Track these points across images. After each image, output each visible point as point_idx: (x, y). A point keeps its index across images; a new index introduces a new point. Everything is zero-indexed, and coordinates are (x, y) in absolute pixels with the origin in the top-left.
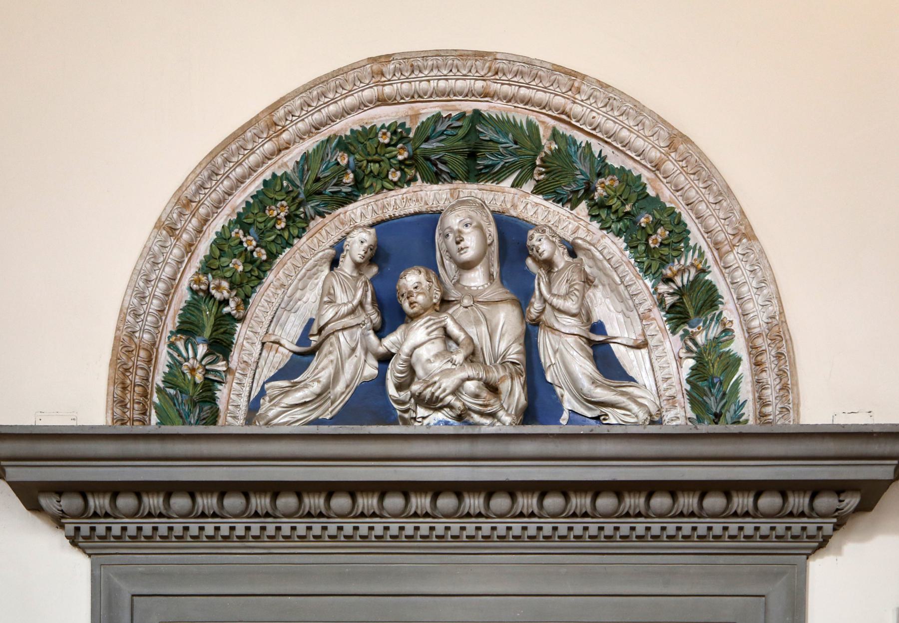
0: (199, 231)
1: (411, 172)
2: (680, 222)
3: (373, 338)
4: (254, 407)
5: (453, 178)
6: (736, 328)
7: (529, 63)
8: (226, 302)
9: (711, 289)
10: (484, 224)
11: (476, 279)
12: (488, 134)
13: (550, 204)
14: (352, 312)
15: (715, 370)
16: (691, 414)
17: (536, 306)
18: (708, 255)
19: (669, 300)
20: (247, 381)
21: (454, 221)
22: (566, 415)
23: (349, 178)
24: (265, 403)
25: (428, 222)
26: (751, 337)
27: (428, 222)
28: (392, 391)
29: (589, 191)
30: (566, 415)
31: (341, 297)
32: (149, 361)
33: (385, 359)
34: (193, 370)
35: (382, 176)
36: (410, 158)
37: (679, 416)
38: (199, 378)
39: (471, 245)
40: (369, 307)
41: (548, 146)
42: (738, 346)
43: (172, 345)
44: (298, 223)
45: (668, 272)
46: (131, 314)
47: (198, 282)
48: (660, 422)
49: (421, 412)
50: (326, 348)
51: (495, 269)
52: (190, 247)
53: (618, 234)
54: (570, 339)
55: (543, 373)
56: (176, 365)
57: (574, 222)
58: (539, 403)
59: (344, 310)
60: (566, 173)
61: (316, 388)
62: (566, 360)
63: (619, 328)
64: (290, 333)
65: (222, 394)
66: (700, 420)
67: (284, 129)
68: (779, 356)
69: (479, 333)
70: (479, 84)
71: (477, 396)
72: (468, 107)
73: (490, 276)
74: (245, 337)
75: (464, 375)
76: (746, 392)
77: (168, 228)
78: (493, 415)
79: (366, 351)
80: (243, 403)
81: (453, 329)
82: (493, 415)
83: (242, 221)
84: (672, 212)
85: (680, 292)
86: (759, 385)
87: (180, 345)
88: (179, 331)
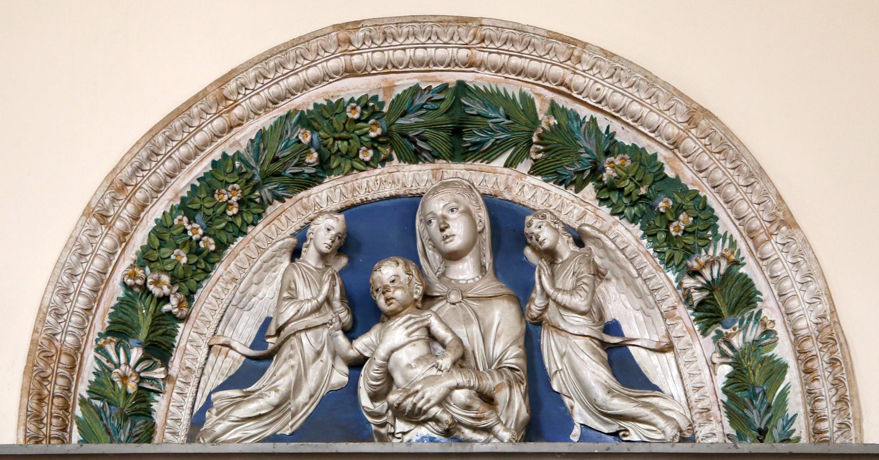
0: (136, 218)
1: (385, 151)
2: (706, 207)
3: (342, 340)
4: (197, 421)
5: (435, 156)
6: (779, 328)
7: (521, 29)
8: (166, 299)
9: (747, 284)
11: (465, 271)
12: (475, 107)
13: (551, 187)
14: (317, 309)
15: (757, 378)
18: (741, 245)
19: (697, 296)
21: (437, 205)
22: (577, 431)
23: (313, 158)
24: (211, 417)
26: (798, 341)
28: (365, 401)
29: (596, 171)
33: (356, 365)
34: (124, 378)
37: (715, 431)
38: (132, 387)
39: (458, 233)
40: (337, 304)
41: (546, 121)
43: (100, 349)
44: (253, 208)
45: (694, 264)
47: (133, 276)
48: (692, 440)
49: (401, 426)
50: (286, 351)
51: (488, 260)
53: (633, 220)
54: (580, 341)
56: (104, 373)
57: (580, 206)
58: (544, 414)
59: (307, 307)
60: (568, 151)
61: (273, 398)
62: (576, 365)
63: (639, 329)
64: (242, 334)
65: (159, 405)
66: (741, 437)
68: (833, 362)
69: (470, 334)
71: (468, 407)
72: (451, 78)
73: (482, 268)
74: (188, 340)
75: (452, 382)
76: (795, 404)
78: (488, 430)
79: (335, 355)
80: (185, 416)
81: (438, 329)
84: (695, 196)
85: (709, 286)
86: (812, 398)
87: (110, 349)
88: (109, 332)
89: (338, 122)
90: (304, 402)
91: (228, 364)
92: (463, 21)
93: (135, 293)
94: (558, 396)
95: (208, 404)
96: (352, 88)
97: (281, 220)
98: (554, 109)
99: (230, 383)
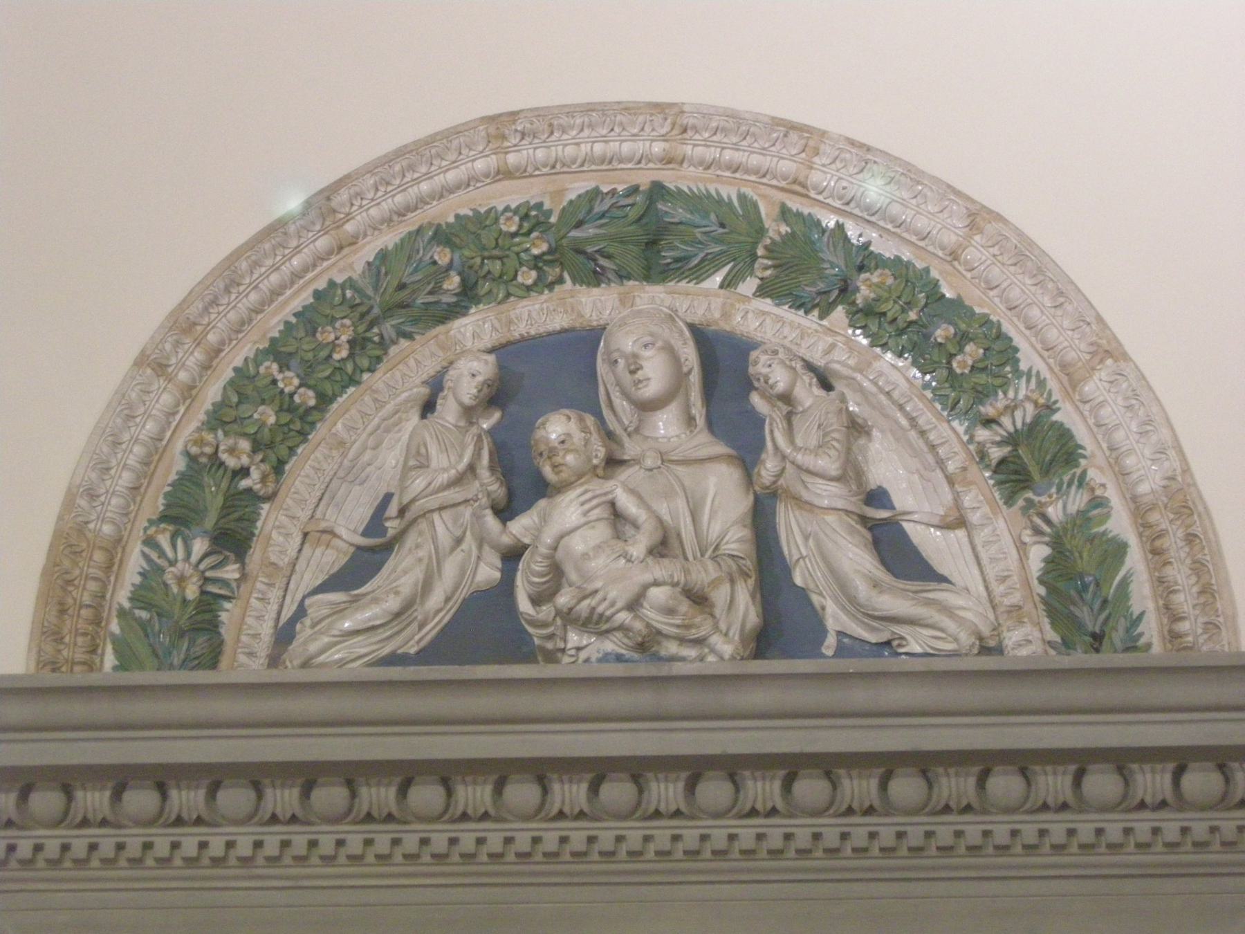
0: (206, 367)
1: (552, 273)
2: (1000, 336)
3: (491, 521)
4: (285, 635)
5: (623, 276)
7: (733, 115)
8: (244, 472)
9: (1064, 435)
10: (677, 344)
11: (665, 425)
13: (785, 312)
14: (458, 481)
15: (1086, 562)
16: (1052, 635)
17: (768, 467)
18: (1052, 384)
19: (996, 453)
20: (274, 595)
22: (831, 640)
24: (304, 630)
25: (582, 345)
26: (1140, 510)
27: (582, 345)
29: (846, 290)
30: (831, 640)
31: (438, 459)
32: (108, 568)
33: (512, 556)
34: (181, 579)
35: (507, 279)
36: (551, 251)
37: (1028, 640)
38: (192, 592)
39: (655, 375)
40: (484, 473)
41: (776, 229)
42: (1120, 524)
43: (150, 542)
44: (369, 349)
45: (988, 410)
46: (83, 494)
47: (200, 442)
48: (999, 650)
49: (574, 638)
50: (411, 539)
51: (698, 410)
52: (189, 393)
54: (831, 518)
55: (787, 571)
56: (152, 574)
57: (834, 338)
58: (783, 622)
59: (444, 478)
60: (810, 267)
61: (393, 604)
62: (829, 556)
64: (349, 520)
65: (228, 614)
67: (348, 217)
68: (1190, 538)
69: (675, 511)
70: (658, 148)
71: (670, 612)
72: (643, 179)
73: (690, 420)
74: (277, 530)
75: (648, 577)
76: (1142, 597)
77: (153, 363)
78: (699, 642)
79: (481, 542)
80: (266, 630)
82: (699, 642)
83: (276, 351)
84: (986, 321)
85: (1012, 440)
86: (1164, 588)
87: (164, 540)
88: (164, 518)
89: (488, 238)
90: (438, 607)
91: (328, 559)
92: (659, 108)
93: (202, 466)
94: (803, 593)
95: (301, 612)
96: (511, 195)
97: (409, 364)
98: (784, 213)
99: (337, 582)
